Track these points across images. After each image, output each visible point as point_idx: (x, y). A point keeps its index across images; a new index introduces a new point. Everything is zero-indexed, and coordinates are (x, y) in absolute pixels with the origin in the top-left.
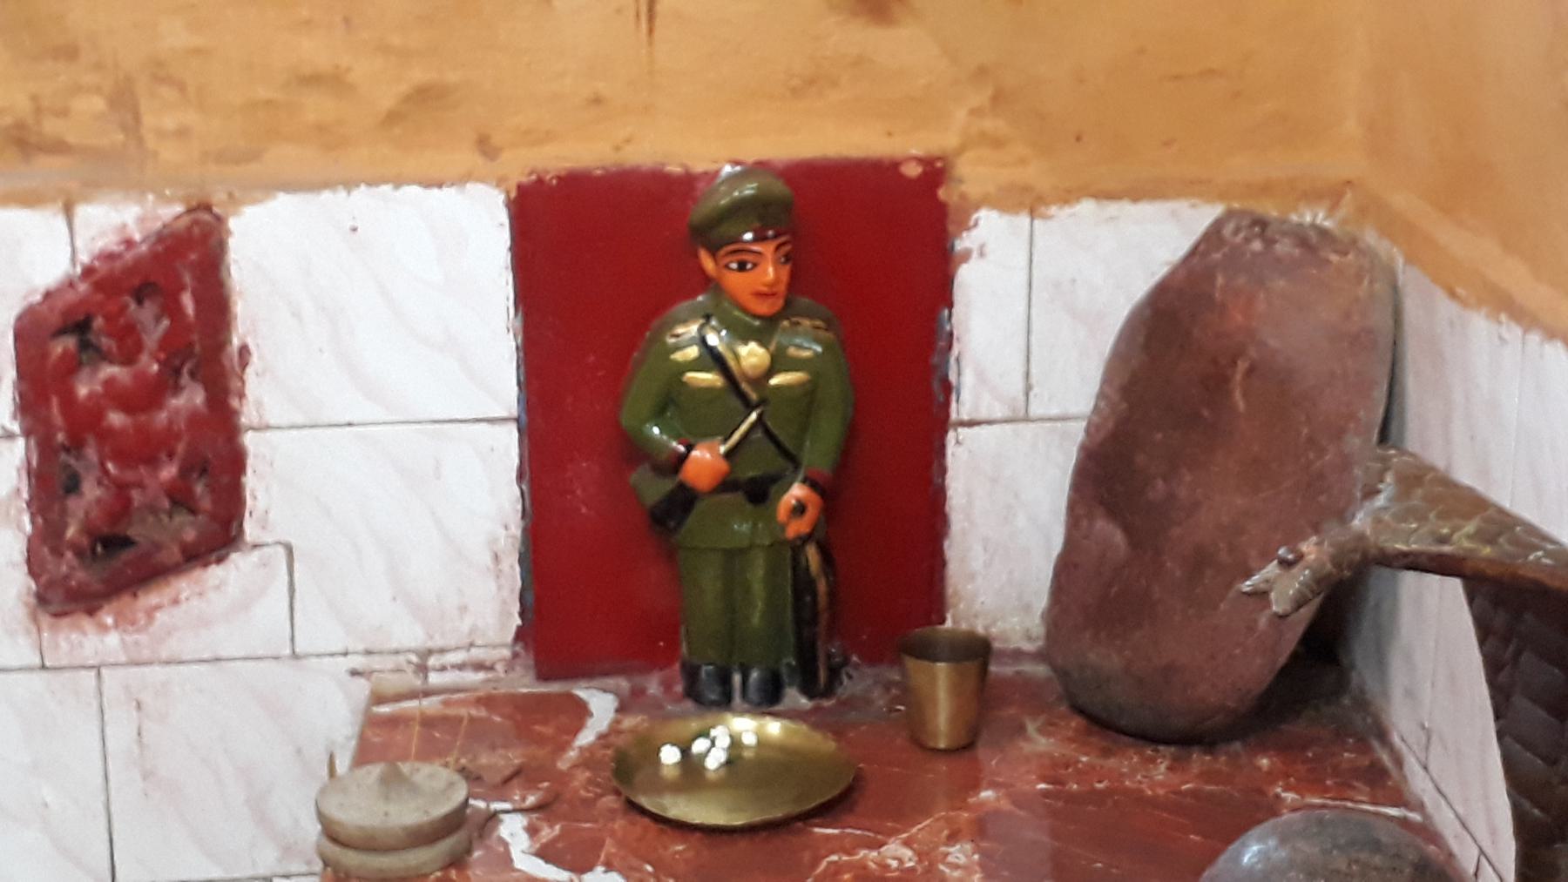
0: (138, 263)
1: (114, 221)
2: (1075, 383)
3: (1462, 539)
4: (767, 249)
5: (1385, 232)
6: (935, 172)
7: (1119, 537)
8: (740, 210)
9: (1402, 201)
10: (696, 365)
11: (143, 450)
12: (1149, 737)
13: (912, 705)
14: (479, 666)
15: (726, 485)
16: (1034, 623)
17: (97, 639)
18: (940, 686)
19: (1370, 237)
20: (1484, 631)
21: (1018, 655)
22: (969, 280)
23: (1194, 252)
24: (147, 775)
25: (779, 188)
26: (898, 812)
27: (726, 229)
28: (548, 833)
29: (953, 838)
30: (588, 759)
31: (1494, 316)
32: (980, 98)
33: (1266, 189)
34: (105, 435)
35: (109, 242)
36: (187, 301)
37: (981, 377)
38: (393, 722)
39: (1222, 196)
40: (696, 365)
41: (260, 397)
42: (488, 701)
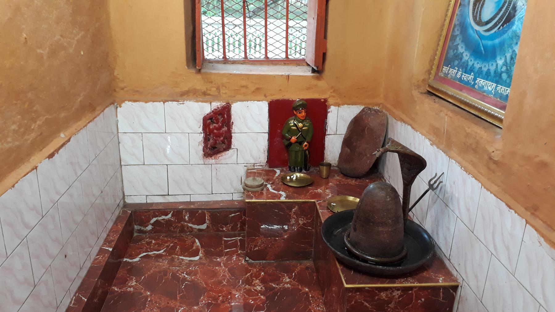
0: (219, 111)
1: (216, 105)
2: (343, 130)
3: (399, 149)
4: (303, 111)
5: (386, 110)
6: (326, 100)
7: (349, 151)
8: (300, 105)
9: (389, 106)
10: (293, 126)
11: (219, 136)
12: (352, 177)
13: (320, 172)
14: (261, 166)
15: (296, 142)
16: (336, 162)
17: (211, 161)
18: (324, 170)
19: (384, 111)
20: (400, 160)
21: (334, 166)
22: (330, 115)
23: (361, 112)
24: (217, 179)
25: (305, 102)
26: (318, 186)
27: (298, 108)
28: (273, 187)
29: (327, 189)
30: (277, 178)
31: (401, 122)
32: (332, 91)
33: (370, 104)
34: (214, 133)
35: (216, 108)
36: (225, 116)
37: (330, 128)
38: (251, 173)
39: (364, 105)
40: (293, 126)
41: (235, 129)
42: (263, 170)
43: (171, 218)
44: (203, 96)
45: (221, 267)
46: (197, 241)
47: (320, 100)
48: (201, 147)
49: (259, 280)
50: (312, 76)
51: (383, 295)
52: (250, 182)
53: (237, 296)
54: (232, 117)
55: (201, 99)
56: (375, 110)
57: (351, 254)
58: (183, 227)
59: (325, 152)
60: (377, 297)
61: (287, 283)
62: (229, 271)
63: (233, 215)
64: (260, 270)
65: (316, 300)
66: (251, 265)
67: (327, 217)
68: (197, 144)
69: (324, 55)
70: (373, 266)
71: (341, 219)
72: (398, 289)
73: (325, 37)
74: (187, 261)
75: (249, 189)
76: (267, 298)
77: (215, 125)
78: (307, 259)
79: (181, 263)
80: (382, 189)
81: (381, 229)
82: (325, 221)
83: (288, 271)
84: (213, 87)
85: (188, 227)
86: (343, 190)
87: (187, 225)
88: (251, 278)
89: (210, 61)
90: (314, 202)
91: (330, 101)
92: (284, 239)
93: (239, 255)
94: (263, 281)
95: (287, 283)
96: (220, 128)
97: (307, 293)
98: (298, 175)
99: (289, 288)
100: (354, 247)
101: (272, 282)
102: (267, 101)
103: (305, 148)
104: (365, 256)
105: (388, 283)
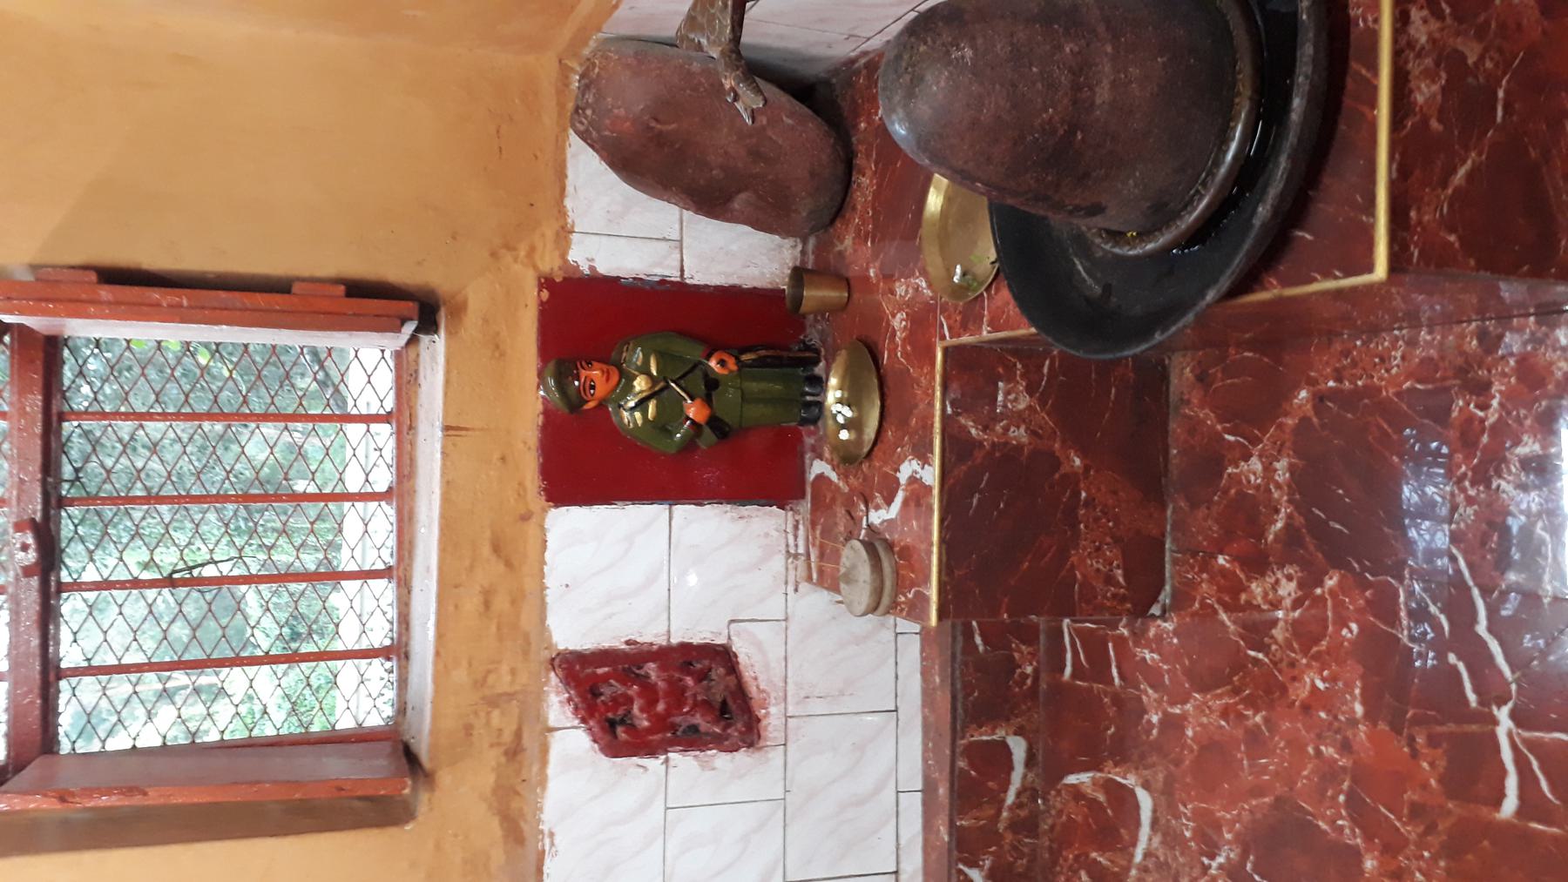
0: (580, 695)
1: (557, 707)
2: (663, 215)
4: (583, 373)
5: (585, 43)
6: (546, 283)
7: (743, 196)
8: (562, 387)
9: (567, 32)
11: (677, 694)
13: (824, 310)
14: (796, 528)
15: (708, 400)
16: (789, 242)
17: (772, 719)
18: (814, 295)
19: (586, 52)
21: (803, 252)
22: (604, 268)
23: (592, 147)
25: (551, 366)
26: (879, 320)
27: (572, 392)
28: (879, 500)
30: (844, 476)
32: (508, 258)
35: (569, 709)
36: (600, 671)
38: (821, 572)
39: (565, 130)
41: (652, 634)
42: (813, 524)
43: (981, 868)
44: (521, 756)
45: (1184, 717)
46: (1072, 779)
47: (542, 303)
48: (721, 760)
49: (1249, 579)
50: (449, 333)
51: (1424, 92)
52: (861, 592)
53: (1320, 685)
54: (606, 645)
55: (535, 769)
56: (585, 89)
57: (1201, 233)
58: (1015, 826)
59: (748, 284)
60: (1435, 124)
61: (1269, 469)
62: (1203, 690)
63: (978, 640)
64: (1206, 565)
65: (1354, 364)
66: (1181, 600)
67: (1013, 309)
68: (709, 774)
69: (358, 289)
70: (1291, 138)
71: (1029, 258)
72: (1402, 20)
73: (279, 286)
74: (1157, 840)
75: (886, 600)
76: (1338, 563)
77: (636, 710)
78: (1164, 377)
79: (1162, 866)
80: (917, 80)
81: (1103, 94)
82: (1033, 321)
83: (1212, 461)
84: (488, 723)
85: (1018, 805)
86: (899, 215)
87: (1010, 809)
88: (1242, 609)
89: (402, 709)
90: (946, 350)
91: (549, 263)
92: (1087, 468)
93: (1139, 636)
94: (1258, 564)
95: (1269, 469)
96: (644, 682)
97: (1319, 399)
98: (833, 395)
99: (1292, 468)
100: (1176, 216)
101: (1261, 535)
102: (545, 511)
103: (732, 365)
104: (1223, 170)
105: (1374, 67)
